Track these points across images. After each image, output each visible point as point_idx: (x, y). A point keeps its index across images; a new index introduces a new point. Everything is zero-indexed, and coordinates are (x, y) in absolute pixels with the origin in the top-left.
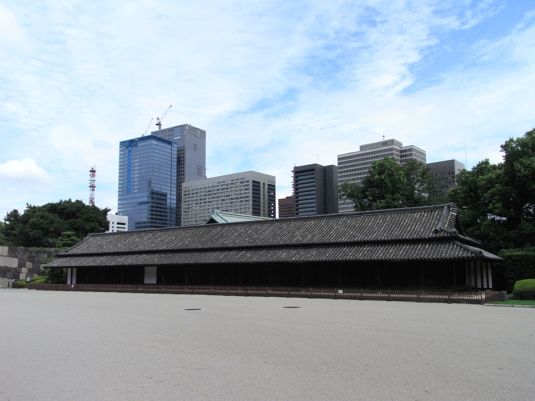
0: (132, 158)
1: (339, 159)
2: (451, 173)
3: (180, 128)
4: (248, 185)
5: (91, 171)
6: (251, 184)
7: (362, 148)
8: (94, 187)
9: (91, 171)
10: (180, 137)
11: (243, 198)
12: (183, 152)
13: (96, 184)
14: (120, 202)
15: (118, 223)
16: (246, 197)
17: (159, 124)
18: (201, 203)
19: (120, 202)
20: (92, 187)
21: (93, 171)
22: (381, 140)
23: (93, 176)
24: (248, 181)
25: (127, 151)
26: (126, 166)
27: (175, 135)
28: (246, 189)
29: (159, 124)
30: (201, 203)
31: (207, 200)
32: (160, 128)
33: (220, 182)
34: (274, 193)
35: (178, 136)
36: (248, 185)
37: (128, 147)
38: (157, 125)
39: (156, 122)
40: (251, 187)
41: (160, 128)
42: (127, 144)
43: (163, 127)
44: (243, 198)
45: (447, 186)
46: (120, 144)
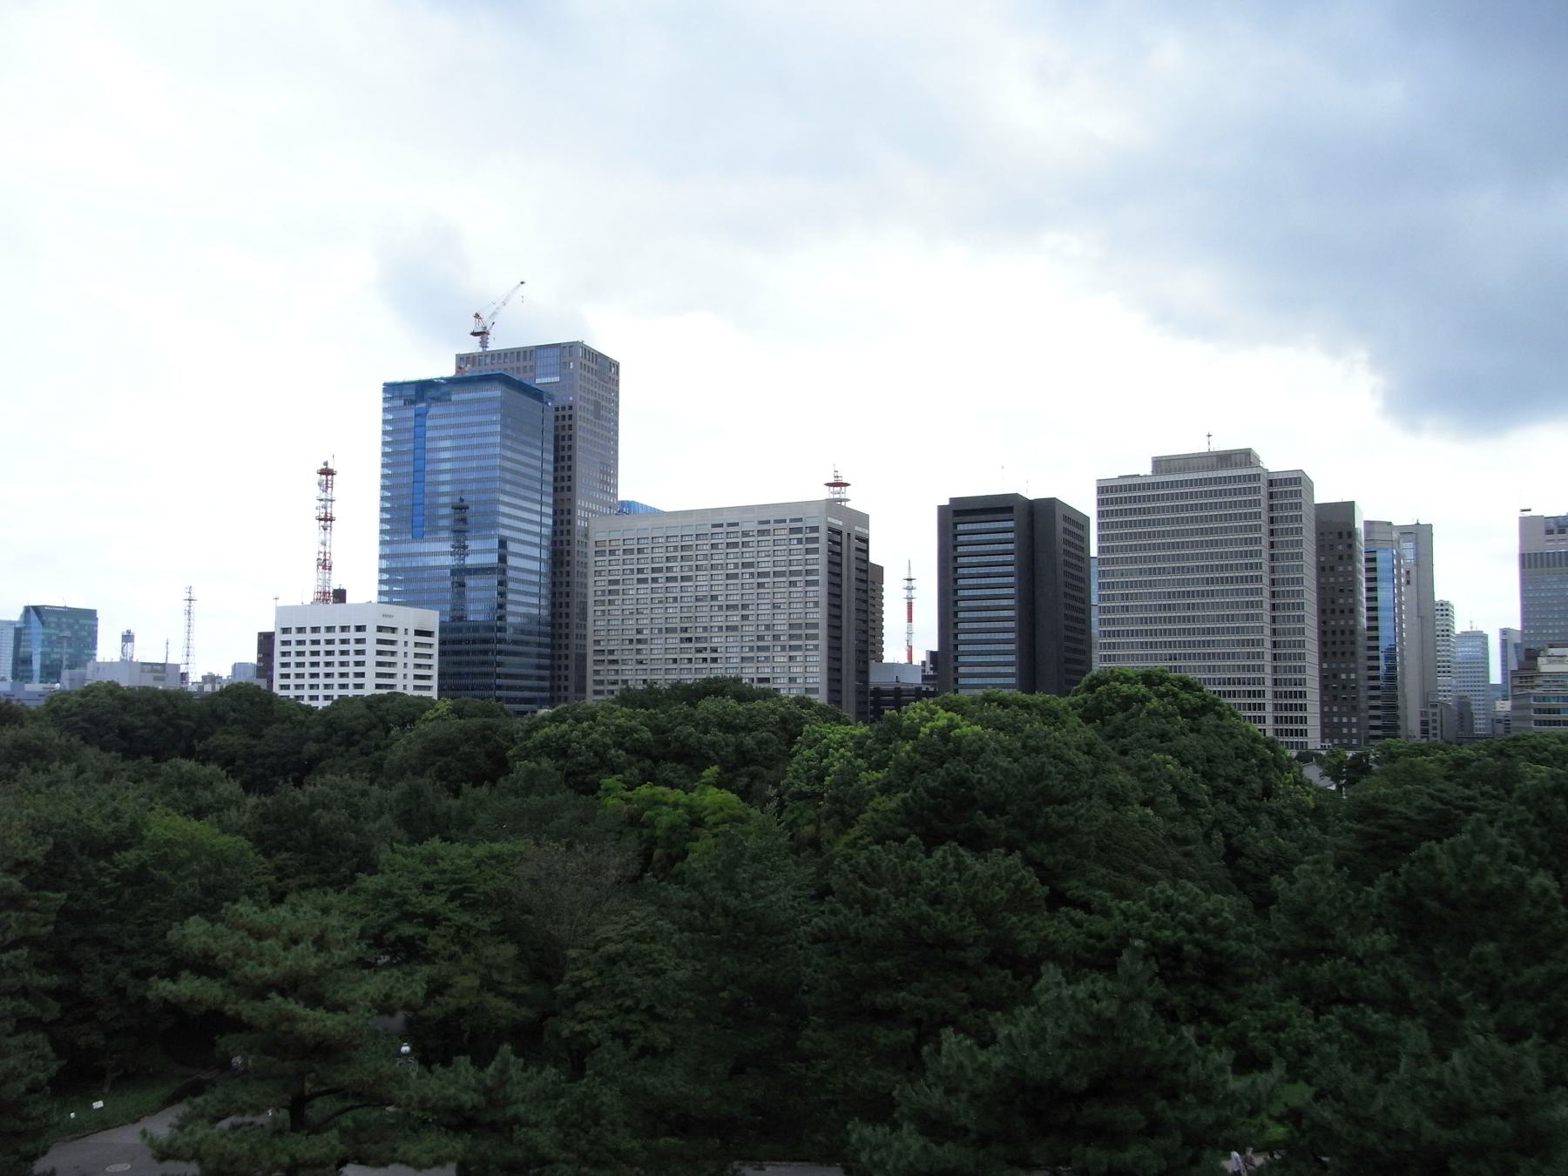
0: (428, 434)
1: (1102, 490)
2: (1345, 535)
3: (556, 352)
4: (816, 540)
5: (322, 472)
6: (823, 535)
7: (1160, 464)
8: (331, 520)
9: (322, 472)
10: (557, 379)
11: (798, 573)
12: (567, 422)
13: (336, 510)
14: (385, 564)
15: (418, 633)
16: (808, 572)
17: (482, 334)
18: (655, 580)
19: (385, 564)
20: (326, 520)
21: (327, 472)
22: (1201, 448)
23: (326, 487)
24: (815, 529)
25: (411, 413)
26: (409, 458)
27: (538, 371)
28: (808, 551)
29: (482, 334)
30: (655, 580)
31: (677, 573)
32: (484, 344)
33: (721, 525)
34: (1320, 665)
35: (553, 375)
36: (816, 540)
37: (413, 402)
38: (474, 334)
39: (474, 326)
40: (823, 545)
41: (484, 344)
42: (411, 392)
43: (494, 345)
44: (798, 573)
45: (1332, 568)
46: (385, 390)
